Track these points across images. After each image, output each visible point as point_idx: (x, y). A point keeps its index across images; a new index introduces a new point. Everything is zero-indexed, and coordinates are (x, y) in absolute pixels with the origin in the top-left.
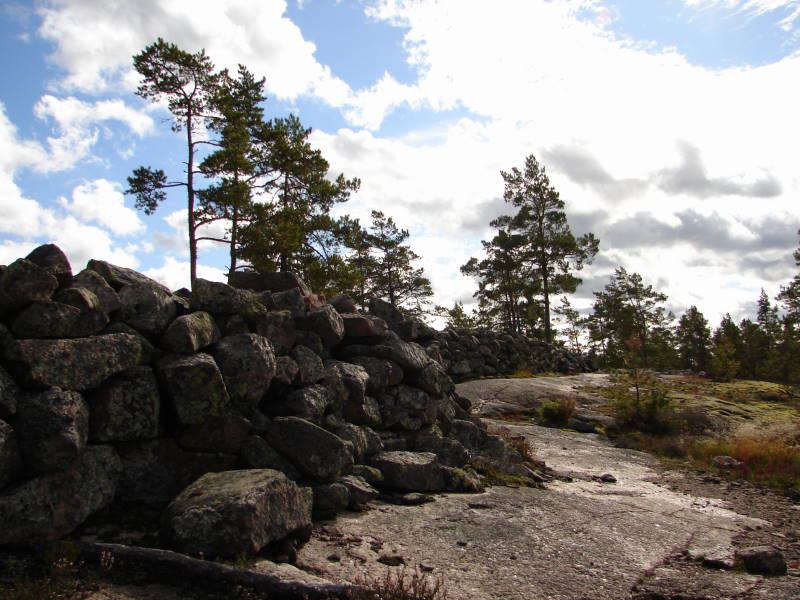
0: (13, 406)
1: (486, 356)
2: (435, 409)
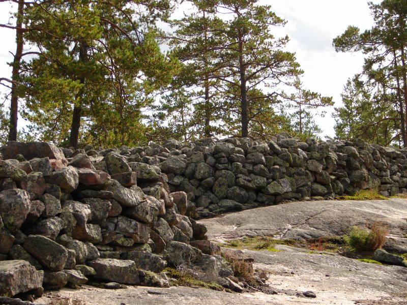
1: (315, 173)
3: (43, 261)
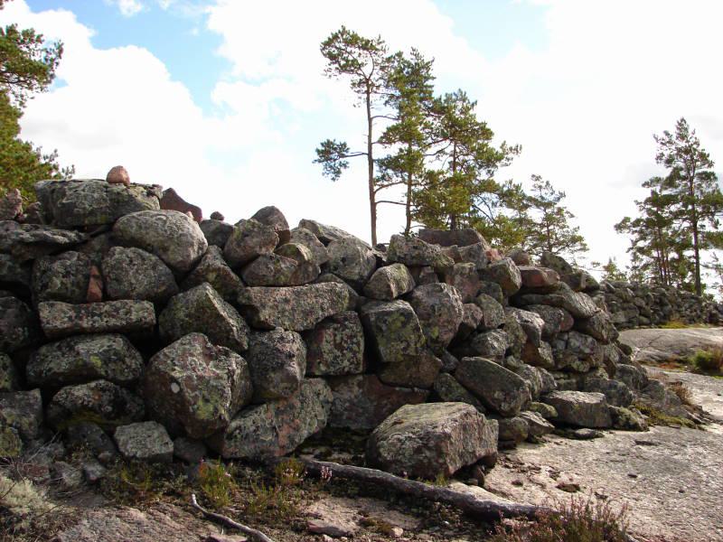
0: (245, 343)
1: (640, 308)
2: (602, 354)
3: (489, 400)
